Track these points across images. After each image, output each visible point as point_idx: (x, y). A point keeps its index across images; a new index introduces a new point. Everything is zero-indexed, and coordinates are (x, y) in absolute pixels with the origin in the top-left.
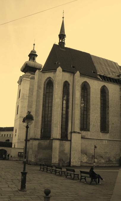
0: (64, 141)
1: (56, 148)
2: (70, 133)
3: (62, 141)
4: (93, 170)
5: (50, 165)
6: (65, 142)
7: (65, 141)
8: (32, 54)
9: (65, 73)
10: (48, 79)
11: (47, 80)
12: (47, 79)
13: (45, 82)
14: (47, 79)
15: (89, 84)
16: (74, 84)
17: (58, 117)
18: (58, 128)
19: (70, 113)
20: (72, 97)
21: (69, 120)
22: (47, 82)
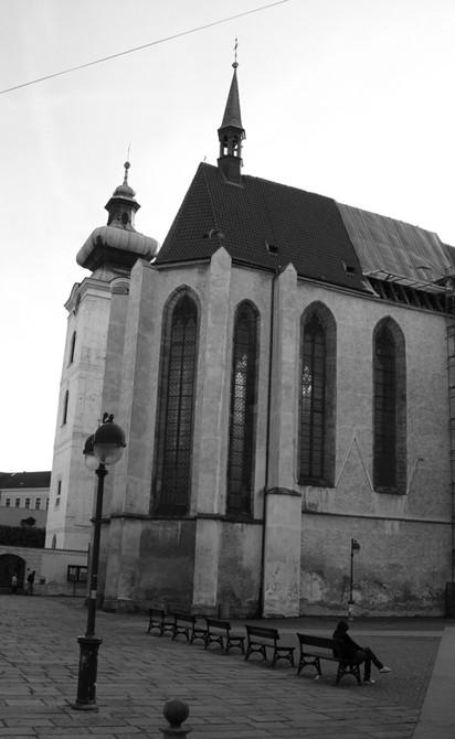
0: (240, 525)
2: (260, 493)
3: (230, 525)
6: (242, 530)
7: (242, 522)
11: (176, 298)
12: (175, 295)
14: (175, 295)
21: (257, 446)
22: (174, 303)
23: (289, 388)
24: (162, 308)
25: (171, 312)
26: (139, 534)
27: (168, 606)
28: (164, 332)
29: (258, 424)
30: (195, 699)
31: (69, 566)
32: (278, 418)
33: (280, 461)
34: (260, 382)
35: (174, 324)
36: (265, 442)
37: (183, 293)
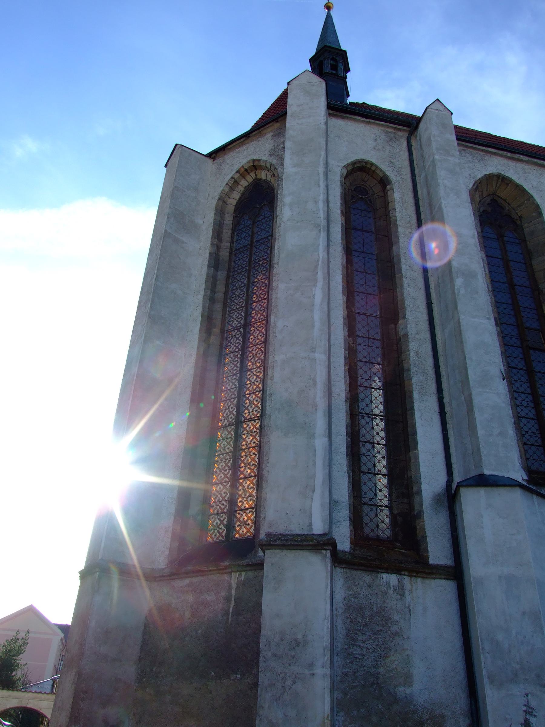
0: (392, 579)
1: (296, 644)
2: (437, 499)
3: (367, 577)
4: (67, 619)
5: (281, 124)
6: (400, 590)
7: (398, 571)
8: (229, 614)
9: (349, 123)
10: (244, 183)
11: (241, 189)
12: (236, 182)
13: (222, 200)
14: (236, 182)
15: (527, 187)
16: (327, 471)
17: (313, 350)
18: (312, 436)
19: (413, 346)
20: (335, 474)
21: (415, 395)
22: (236, 196)
23: (469, 275)
24: (213, 203)
25: (231, 208)
26: (423, 225)
27: (347, 594)
28: (217, 234)
29: (412, 354)
30: (484, 664)
31: (438, 100)
32: (330, 569)
33: (480, 418)
34: (405, 281)
35: (235, 228)
36: (432, 387)
37: (250, 178)
